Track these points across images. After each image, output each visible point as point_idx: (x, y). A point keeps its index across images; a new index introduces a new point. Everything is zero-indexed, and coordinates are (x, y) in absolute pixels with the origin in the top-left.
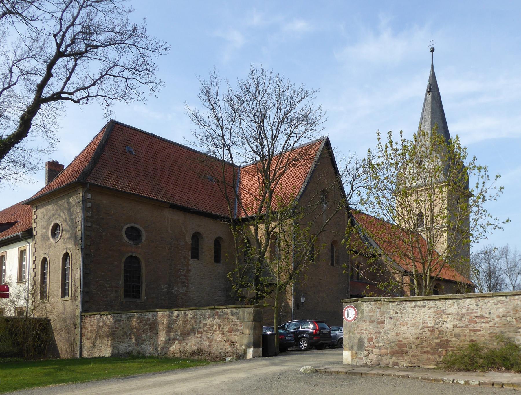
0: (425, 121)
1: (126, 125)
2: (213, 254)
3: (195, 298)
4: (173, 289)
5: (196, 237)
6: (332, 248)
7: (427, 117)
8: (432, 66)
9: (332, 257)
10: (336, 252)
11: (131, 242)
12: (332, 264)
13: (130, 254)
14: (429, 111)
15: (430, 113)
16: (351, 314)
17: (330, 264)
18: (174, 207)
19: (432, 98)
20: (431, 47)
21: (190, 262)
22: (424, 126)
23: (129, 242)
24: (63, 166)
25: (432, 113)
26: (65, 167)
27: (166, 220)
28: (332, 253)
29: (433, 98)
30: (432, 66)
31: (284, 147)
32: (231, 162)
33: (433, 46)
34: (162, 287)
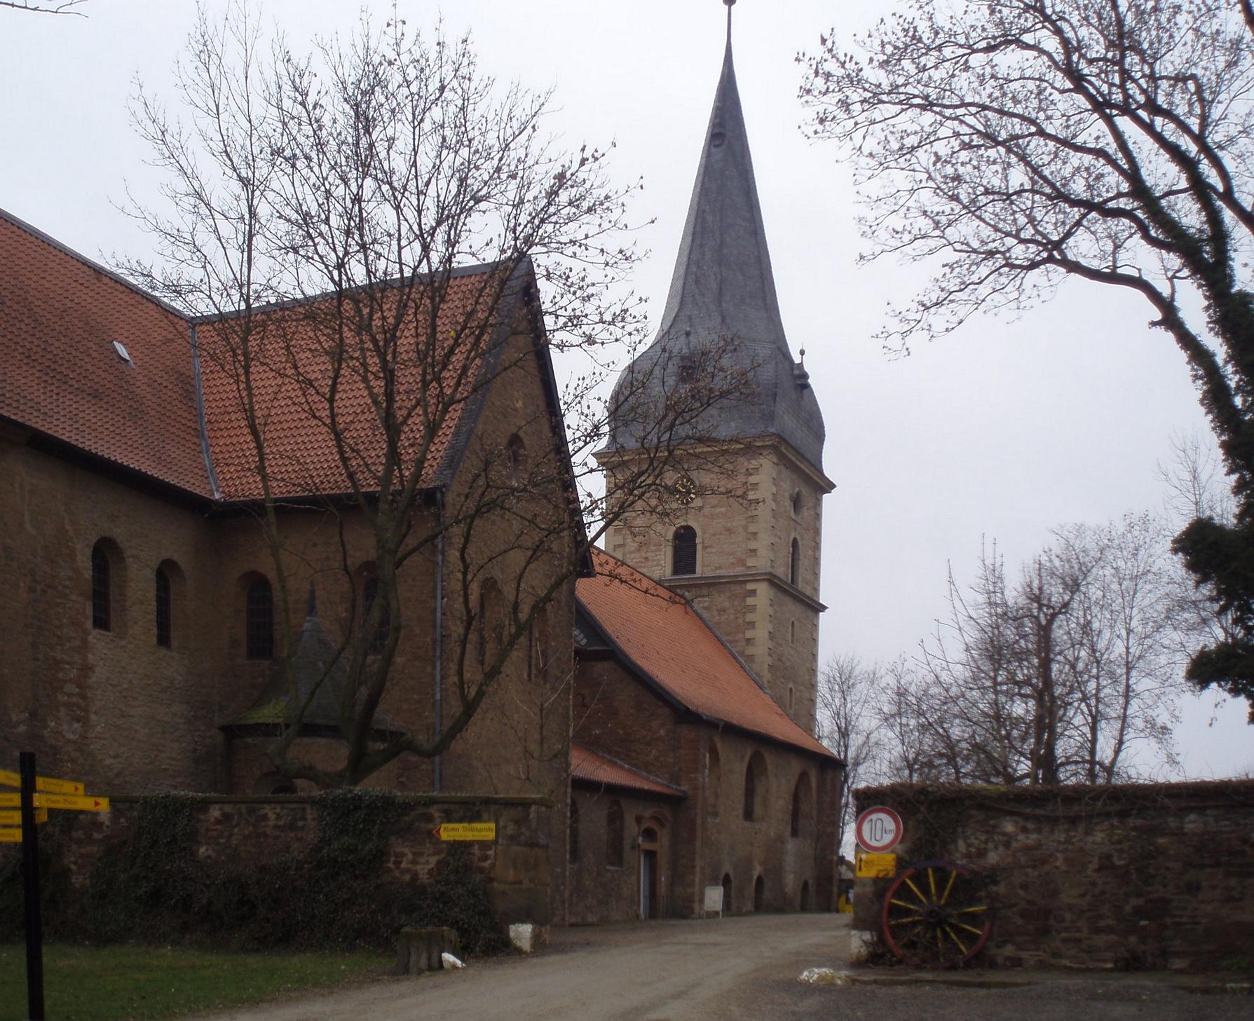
1: (49, 238)
2: (153, 617)
3: (108, 762)
16: (884, 831)
21: (90, 638)
32: (217, 312)
34: (15, 719)
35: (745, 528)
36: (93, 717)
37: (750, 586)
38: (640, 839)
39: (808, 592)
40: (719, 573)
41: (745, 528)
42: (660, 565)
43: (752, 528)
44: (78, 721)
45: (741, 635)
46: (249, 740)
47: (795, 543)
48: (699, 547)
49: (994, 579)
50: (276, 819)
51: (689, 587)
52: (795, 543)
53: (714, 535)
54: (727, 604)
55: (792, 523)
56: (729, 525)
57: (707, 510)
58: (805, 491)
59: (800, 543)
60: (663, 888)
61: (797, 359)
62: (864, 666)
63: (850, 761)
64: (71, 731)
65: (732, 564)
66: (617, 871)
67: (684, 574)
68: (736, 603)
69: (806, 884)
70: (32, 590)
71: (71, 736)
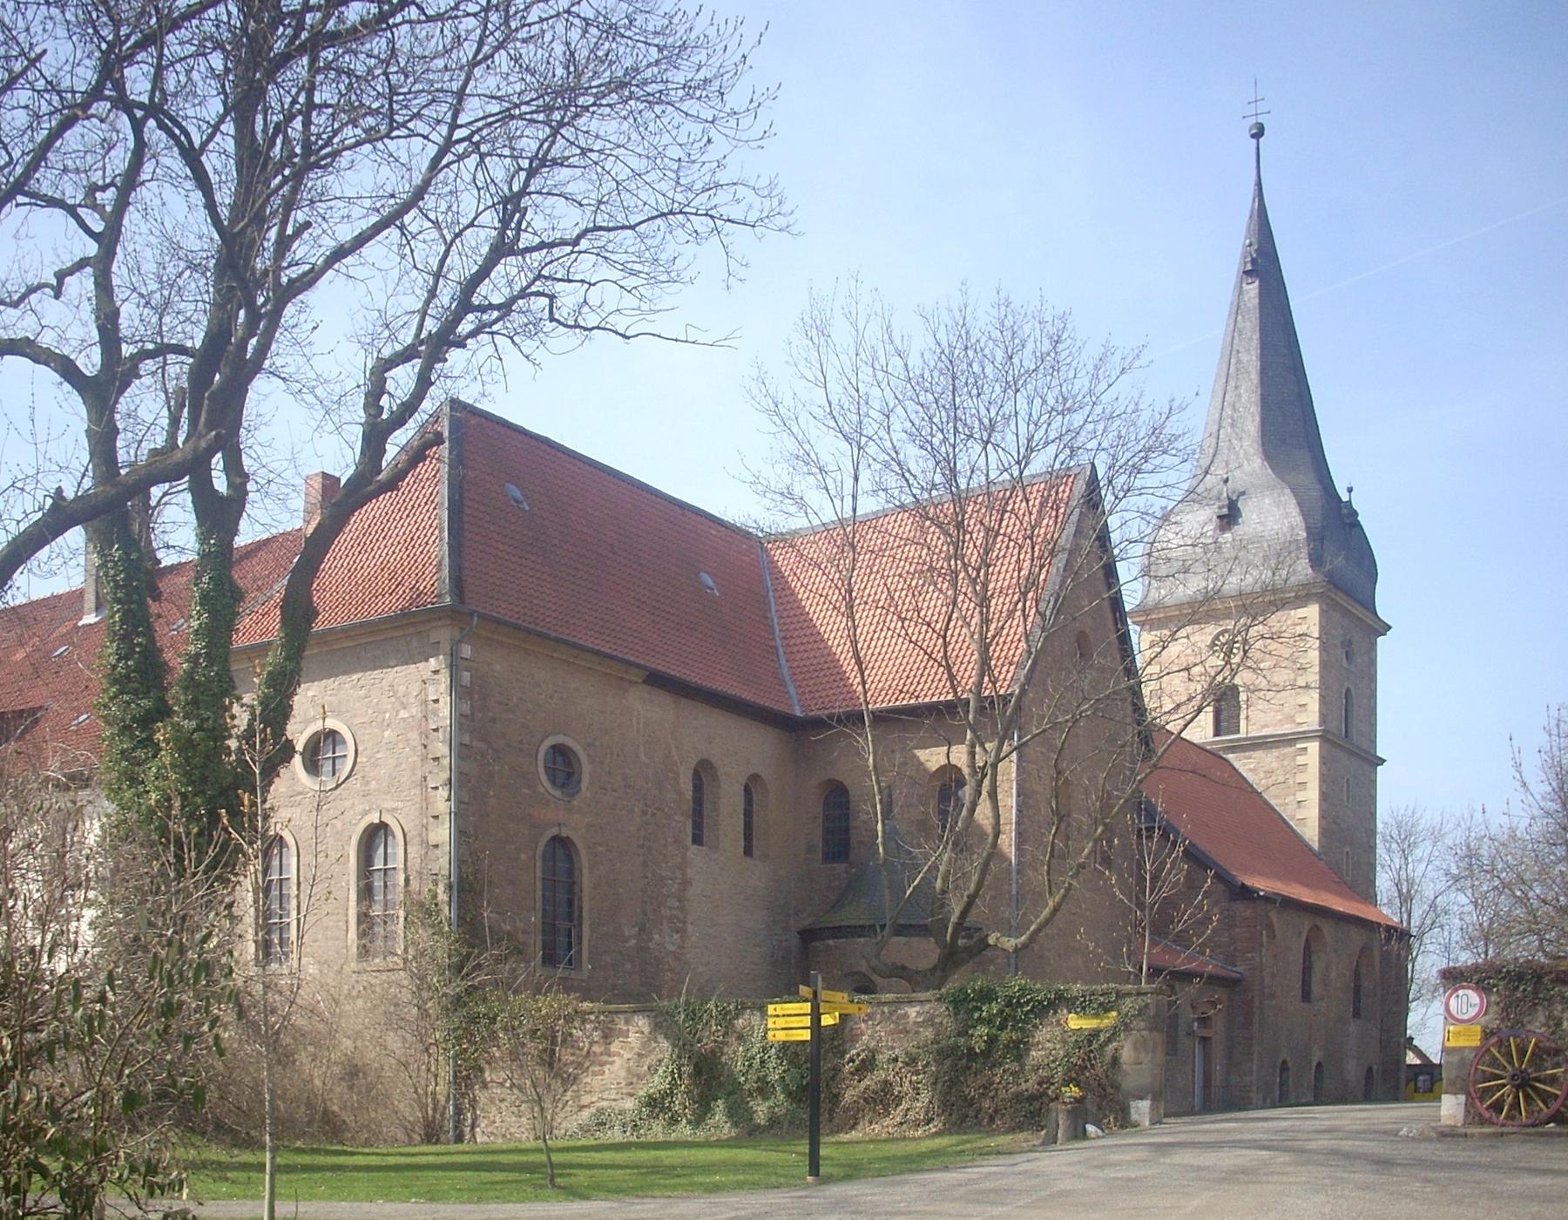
4: (651, 940)
5: (703, 774)
7: (1244, 358)
11: (557, 793)
13: (554, 831)
18: (658, 681)
19: (1260, 293)
20: (1253, 121)
21: (690, 854)
22: (1236, 387)
23: (552, 791)
24: (339, 480)
25: (1264, 346)
26: (343, 482)
27: (634, 721)
29: (1264, 295)
31: (541, 146)
36: (690, 928)
38: (1196, 1024)
40: (1265, 732)
44: (678, 932)
45: (1292, 798)
46: (831, 942)
47: (1348, 691)
52: (1348, 691)
54: (1274, 765)
59: (1353, 693)
60: (1217, 1079)
61: (1345, 498)
62: (1428, 819)
63: (1414, 931)
64: (671, 942)
67: (1228, 734)
68: (1286, 763)
69: (1370, 1070)
70: (644, 813)
71: (671, 948)
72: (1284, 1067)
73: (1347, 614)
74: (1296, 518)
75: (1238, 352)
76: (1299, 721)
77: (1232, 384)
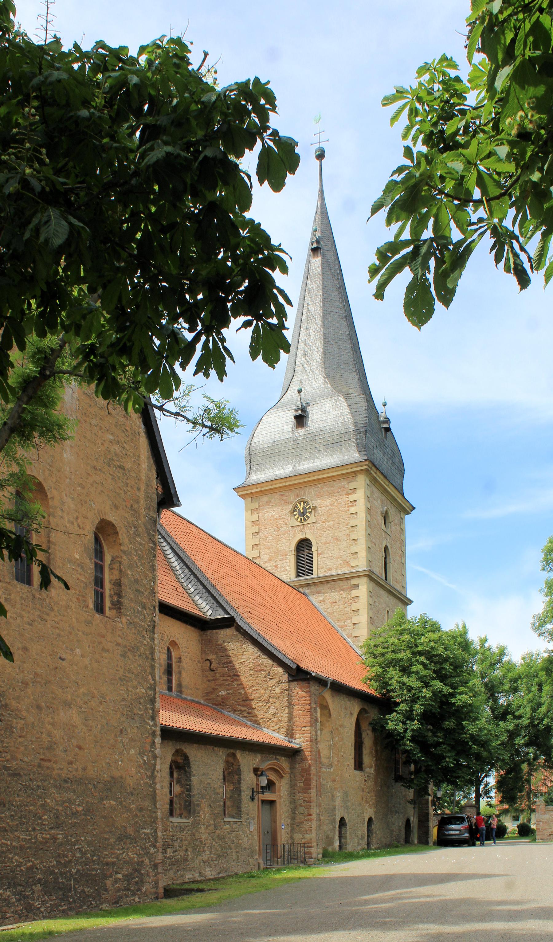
0: (308, 317)
6: (99, 553)
7: (312, 308)
8: (322, 191)
9: (99, 582)
10: (111, 569)
12: (100, 608)
14: (316, 295)
15: (319, 298)
17: (91, 606)
20: (317, 146)
28: (99, 568)
29: (326, 265)
30: (322, 191)
32: (452, 220)
33: (322, 145)
35: (348, 535)
37: (354, 582)
39: (398, 588)
41: (348, 535)
42: (286, 570)
43: (353, 537)
47: (386, 548)
48: (315, 554)
49: (427, 229)
50: (435, 796)
51: (308, 585)
52: (386, 548)
53: (325, 544)
54: (337, 597)
55: (383, 533)
56: (336, 534)
57: (319, 524)
58: (392, 512)
65: (340, 565)
66: (235, 823)
68: (344, 596)
72: (342, 822)
73: (385, 491)
74: (348, 417)
75: (308, 304)
76: (352, 564)
77: (304, 326)
